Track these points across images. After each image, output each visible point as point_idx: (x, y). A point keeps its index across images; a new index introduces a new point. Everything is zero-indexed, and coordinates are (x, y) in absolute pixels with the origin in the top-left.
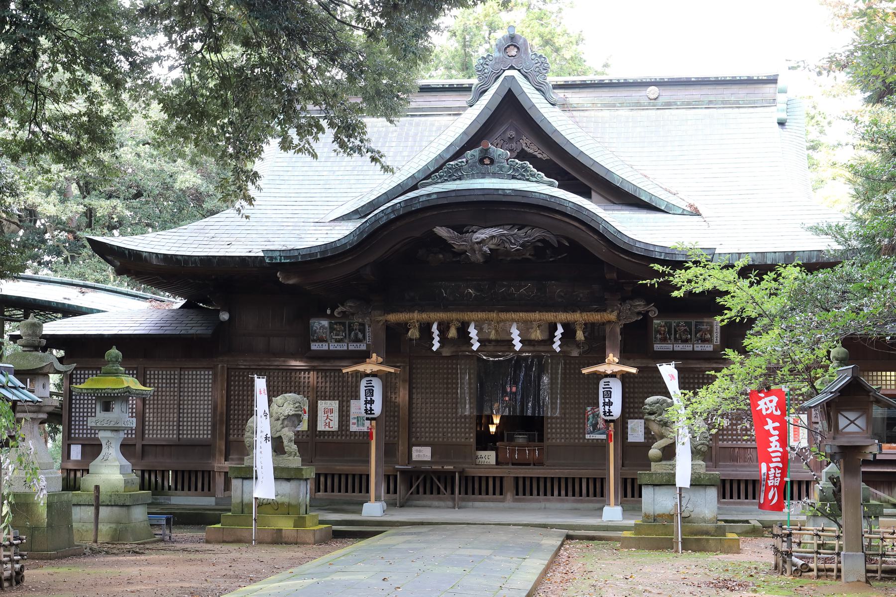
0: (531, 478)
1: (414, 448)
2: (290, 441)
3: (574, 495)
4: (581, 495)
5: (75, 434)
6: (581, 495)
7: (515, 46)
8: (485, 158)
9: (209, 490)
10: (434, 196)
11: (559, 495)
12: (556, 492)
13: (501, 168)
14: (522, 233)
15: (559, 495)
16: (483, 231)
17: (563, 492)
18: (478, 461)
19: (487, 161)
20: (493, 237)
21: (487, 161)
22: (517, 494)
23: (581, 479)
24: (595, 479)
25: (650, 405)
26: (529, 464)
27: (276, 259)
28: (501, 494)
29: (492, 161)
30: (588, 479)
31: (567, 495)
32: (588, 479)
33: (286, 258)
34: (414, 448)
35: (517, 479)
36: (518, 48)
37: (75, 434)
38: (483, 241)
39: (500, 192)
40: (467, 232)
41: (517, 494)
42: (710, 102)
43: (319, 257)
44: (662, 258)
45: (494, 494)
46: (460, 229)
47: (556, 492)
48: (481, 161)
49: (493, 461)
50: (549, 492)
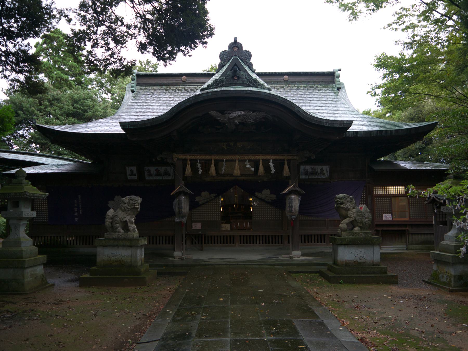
0: (247, 236)
1: (193, 224)
2: (435, 192)
3: (266, 243)
4: (269, 243)
5: (194, 218)
6: (269, 243)
7: (237, 47)
8: (235, 76)
9: (92, 244)
10: (211, 94)
11: (260, 243)
12: (258, 242)
13: (243, 81)
14: (254, 114)
15: (260, 243)
16: (234, 113)
17: (261, 242)
18: (222, 229)
19: (236, 78)
20: (239, 116)
21: (236, 78)
22: (241, 243)
23: (269, 236)
24: (275, 236)
25: (340, 199)
26: (246, 230)
27: (126, 126)
28: (233, 243)
29: (239, 78)
30: (272, 236)
31: (263, 243)
32: (272, 236)
33: (131, 126)
34: (193, 224)
35: (240, 236)
36: (238, 48)
37: (194, 218)
38: (235, 118)
39: (244, 92)
40: (226, 114)
41: (241, 243)
42: (309, 82)
43: (149, 125)
44: (327, 125)
45: (230, 243)
46: (223, 112)
47: (258, 242)
48: (233, 77)
49: (229, 228)
50: (255, 242)
